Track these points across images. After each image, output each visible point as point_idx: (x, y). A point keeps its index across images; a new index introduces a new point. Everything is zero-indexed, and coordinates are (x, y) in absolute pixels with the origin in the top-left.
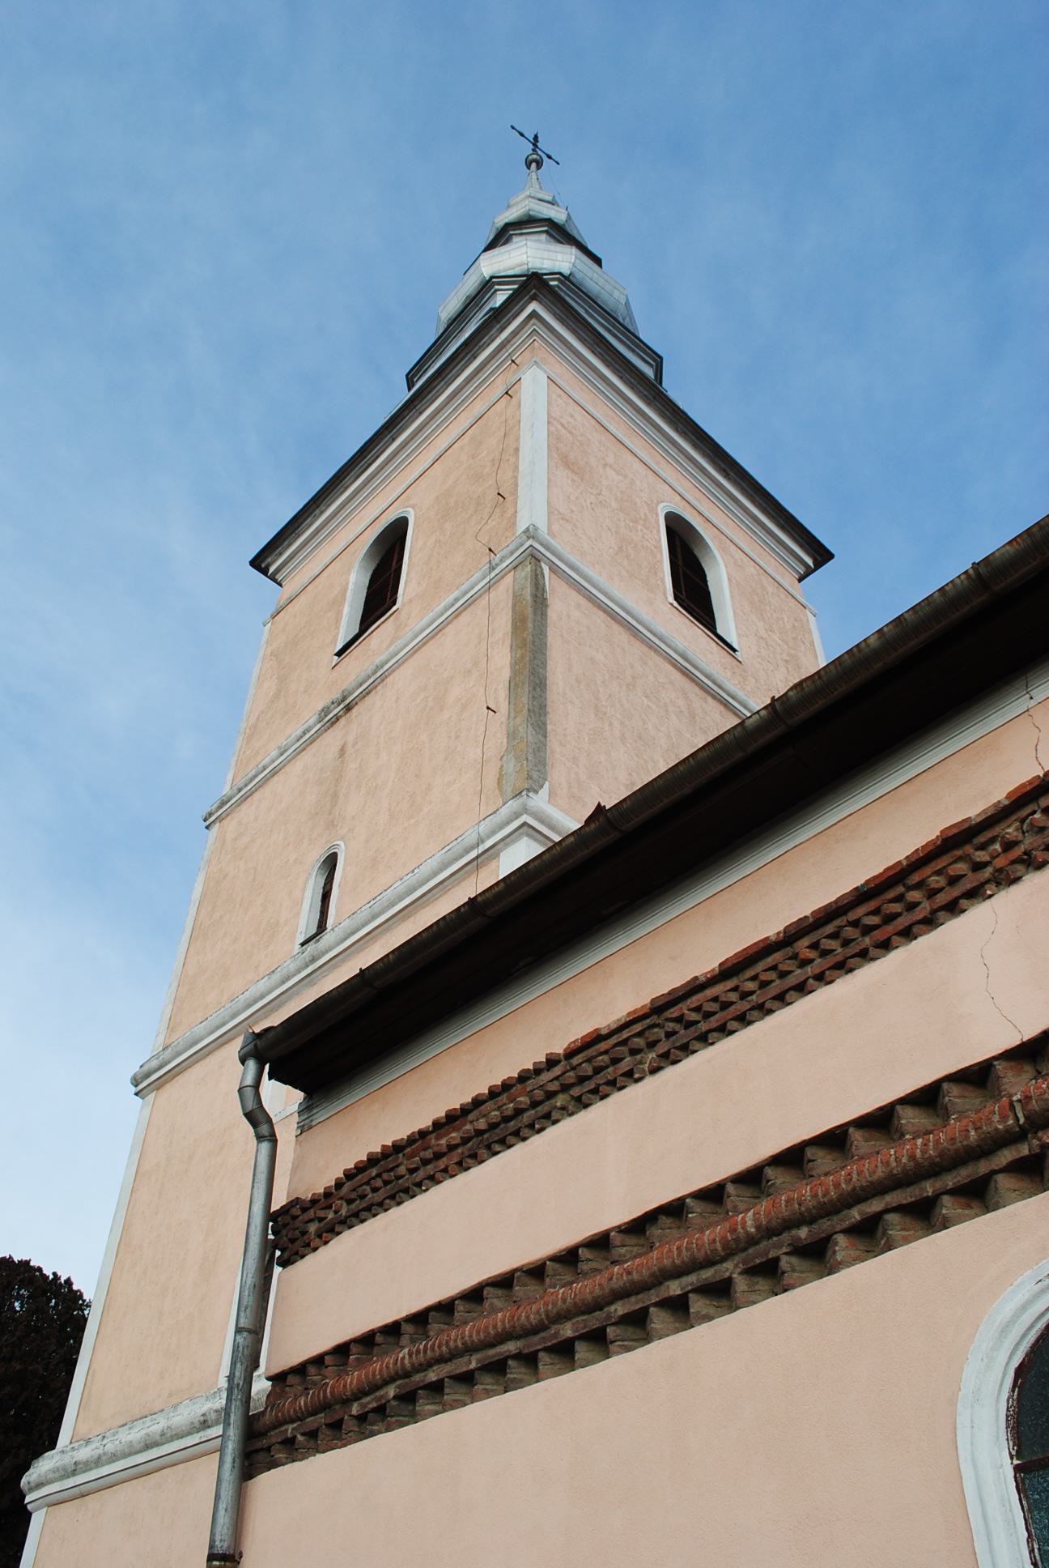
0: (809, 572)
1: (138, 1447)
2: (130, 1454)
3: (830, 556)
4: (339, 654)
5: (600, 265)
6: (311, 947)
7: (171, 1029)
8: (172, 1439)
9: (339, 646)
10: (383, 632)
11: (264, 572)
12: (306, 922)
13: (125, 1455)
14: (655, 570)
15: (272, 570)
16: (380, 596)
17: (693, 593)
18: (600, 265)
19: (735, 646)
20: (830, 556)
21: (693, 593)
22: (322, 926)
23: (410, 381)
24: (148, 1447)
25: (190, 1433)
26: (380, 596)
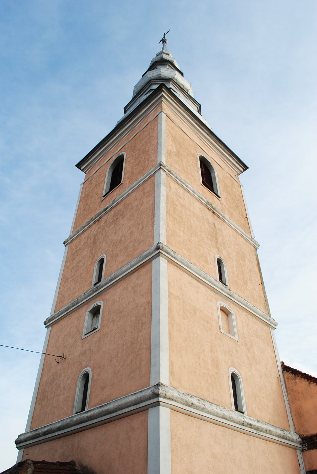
0: (242, 172)
1: (220, 416)
2: (216, 416)
3: (248, 168)
4: (104, 196)
5: (183, 76)
6: (96, 286)
7: (55, 312)
8: (232, 421)
9: (104, 194)
10: (118, 193)
11: (80, 169)
12: (94, 279)
13: (213, 415)
14: (198, 172)
15: (82, 168)
16: (116, 180)
17: (208, 180)
18: (183, 76)
19: (219, 195)
20: (248, 168)
21: (208, 180)
22: (99, 280)
23: (125, 110)
24: (223, 418)
25: (237, 423)
26: (116, 180)
